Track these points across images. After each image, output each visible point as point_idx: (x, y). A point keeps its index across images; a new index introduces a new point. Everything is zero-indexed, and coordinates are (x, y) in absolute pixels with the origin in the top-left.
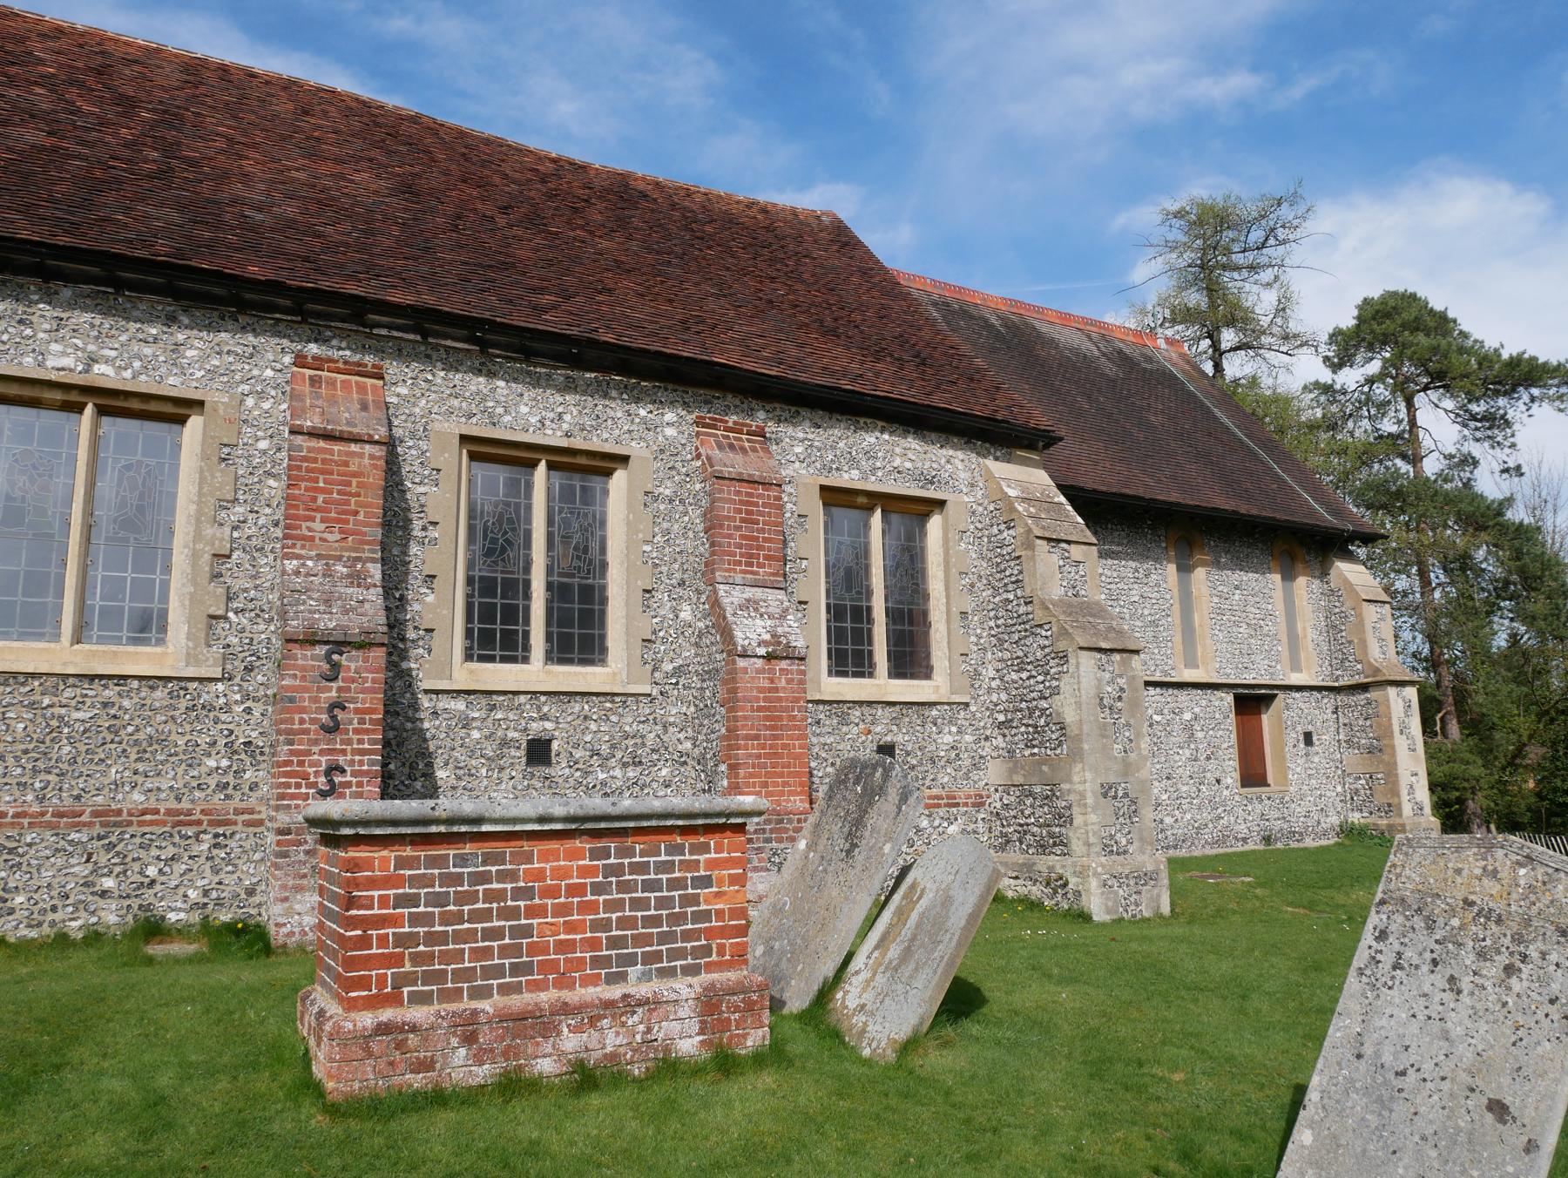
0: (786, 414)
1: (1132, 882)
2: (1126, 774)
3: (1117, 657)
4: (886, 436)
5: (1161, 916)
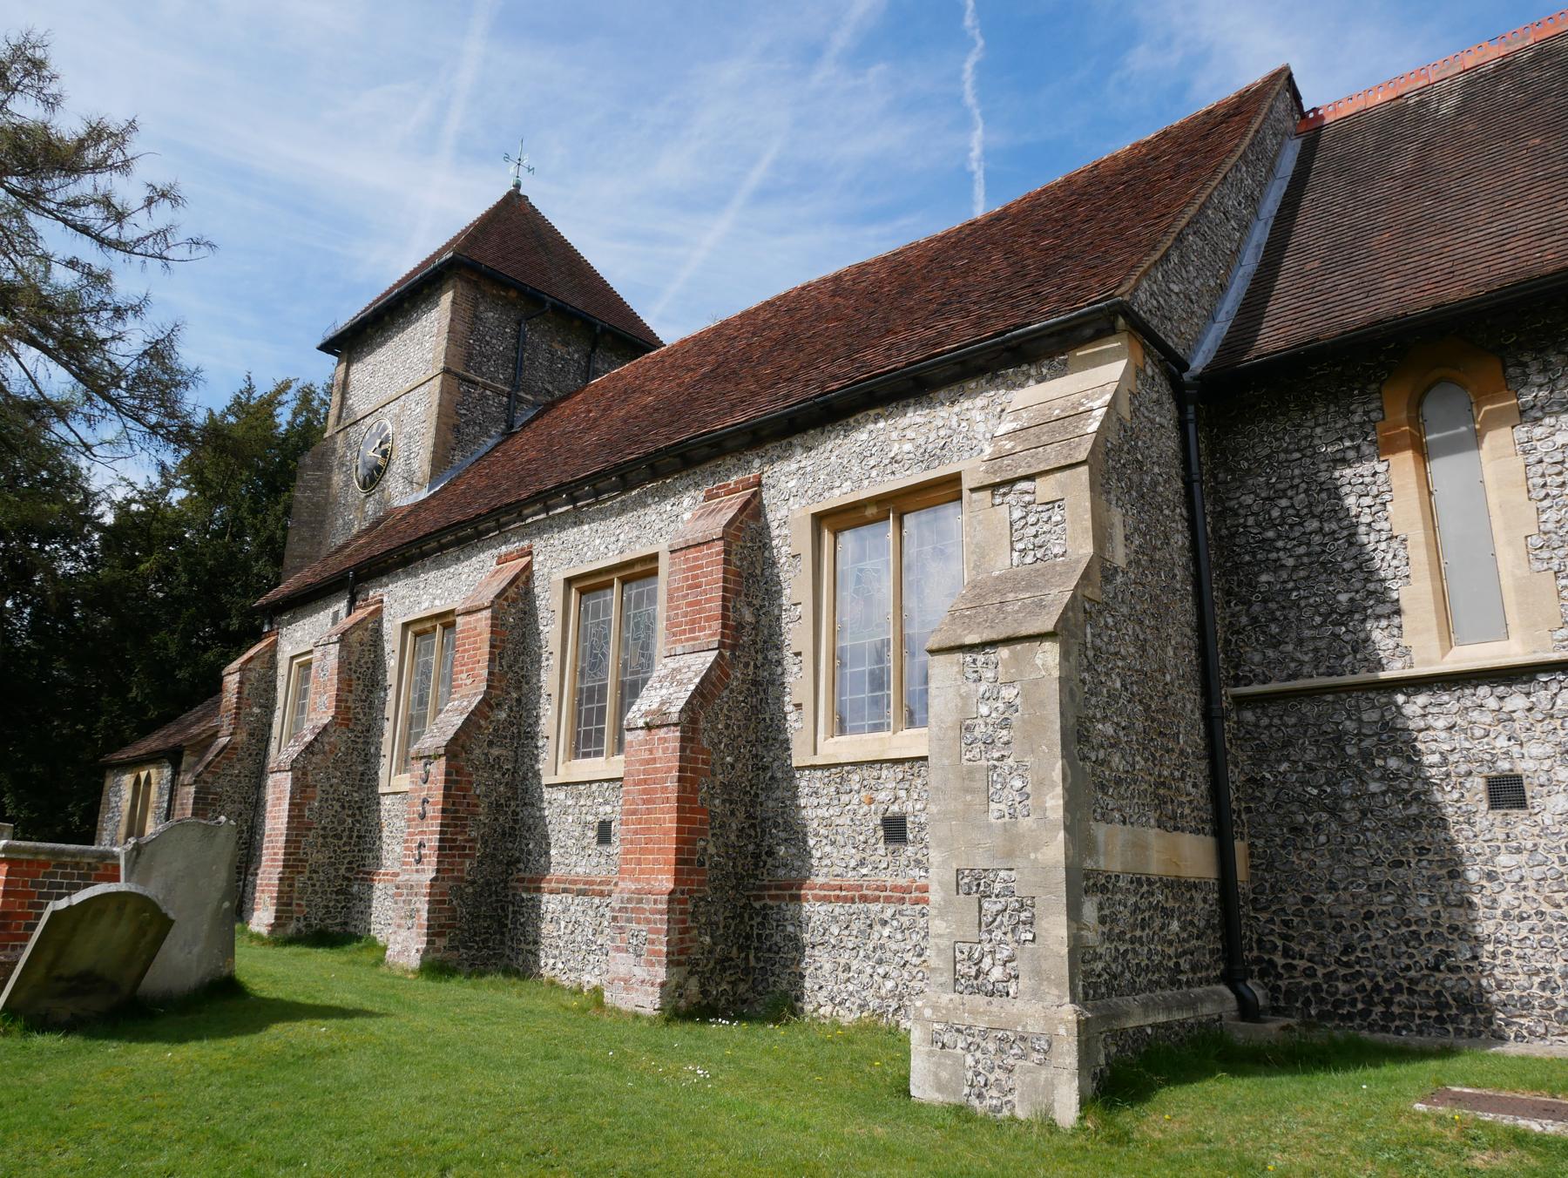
0: (778, 452)
1: (992, 1047)
2: (1010, 854)
3: (1004, 652)
4: (881, 424)
5: (1051, 1127)
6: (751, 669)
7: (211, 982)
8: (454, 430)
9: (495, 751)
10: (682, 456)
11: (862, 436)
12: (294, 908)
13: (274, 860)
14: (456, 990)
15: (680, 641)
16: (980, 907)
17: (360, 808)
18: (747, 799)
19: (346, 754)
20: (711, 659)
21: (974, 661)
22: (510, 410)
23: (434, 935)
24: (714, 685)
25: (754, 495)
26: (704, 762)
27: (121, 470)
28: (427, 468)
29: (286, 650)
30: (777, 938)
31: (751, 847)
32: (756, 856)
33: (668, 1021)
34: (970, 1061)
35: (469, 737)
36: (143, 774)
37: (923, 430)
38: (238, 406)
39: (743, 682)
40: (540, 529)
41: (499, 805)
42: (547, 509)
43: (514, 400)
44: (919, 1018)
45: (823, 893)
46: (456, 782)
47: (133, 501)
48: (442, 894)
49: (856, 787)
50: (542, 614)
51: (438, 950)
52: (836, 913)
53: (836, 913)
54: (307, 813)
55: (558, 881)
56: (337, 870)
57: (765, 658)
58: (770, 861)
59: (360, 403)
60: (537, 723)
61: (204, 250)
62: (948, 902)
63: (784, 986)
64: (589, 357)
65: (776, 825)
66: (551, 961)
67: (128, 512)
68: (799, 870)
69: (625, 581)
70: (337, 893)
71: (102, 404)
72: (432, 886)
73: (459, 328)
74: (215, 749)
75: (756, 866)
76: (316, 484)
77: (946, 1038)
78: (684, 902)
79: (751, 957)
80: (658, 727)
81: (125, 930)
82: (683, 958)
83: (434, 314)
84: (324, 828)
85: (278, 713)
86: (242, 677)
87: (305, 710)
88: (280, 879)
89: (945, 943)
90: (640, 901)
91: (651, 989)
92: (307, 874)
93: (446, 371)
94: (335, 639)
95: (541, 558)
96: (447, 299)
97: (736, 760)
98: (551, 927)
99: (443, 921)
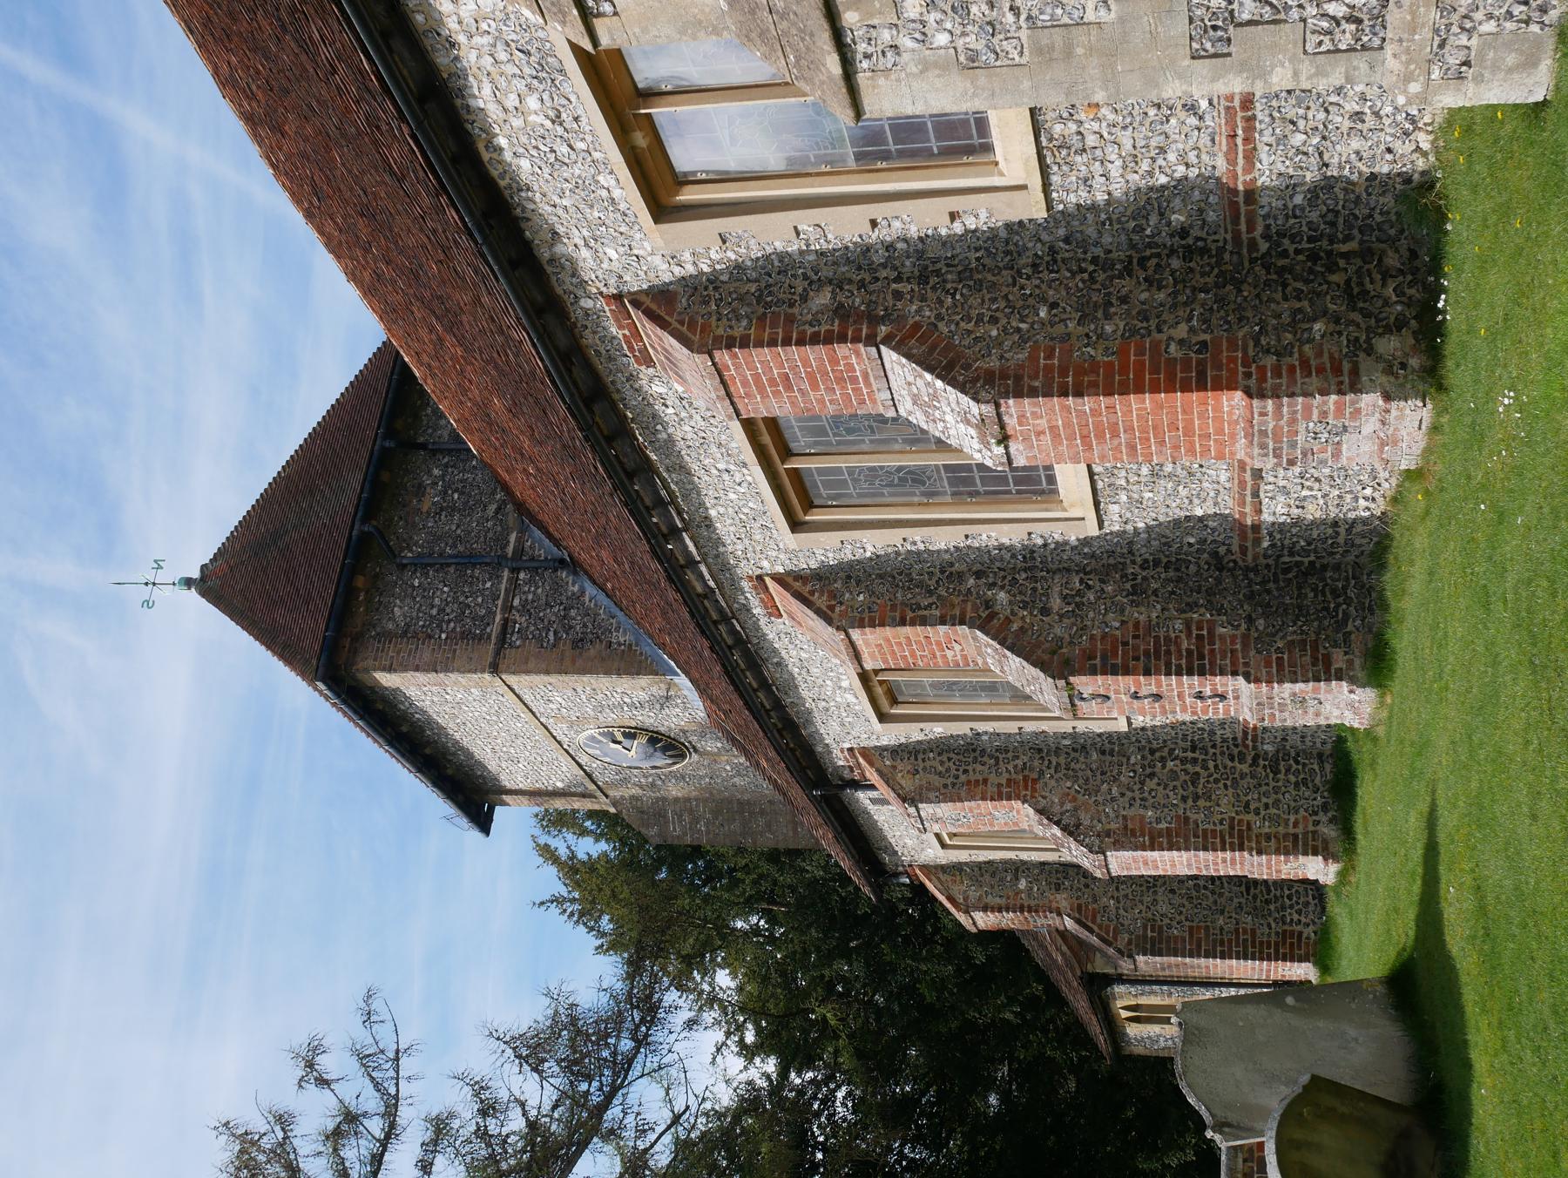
3: (850, 18)
4: (502, 141)
6: (904, 287)
7: (1396, 1008)
8: (582, 648)
9: (1056, 603)
10: (588, 402)
11: (525, 167)
12: (1300, 830)
13: (1233, 861)
14: (1405, 642)
15: (870, 394)
16: (1250, 23)
17: (1152, 752)
18: (1101, 277)
19: (1075, 779)
20: (895, 356)
21: (867, 56)
22: (537, 567)
23: (1327, 670)
24: (933, 348)
25: (636, 304)
26: (1050, 356)
27: (705, 1064)
28: (644, 681)
29: (933, 853)
30: (1314, 216)
31: (1175, 263)
32: (1189, 253)
33: (1441, 388)
34: (1490, 27)
35: (1038, 645)
36: (1124, 1014)
37: (502, 83)
38: (586, 915)
39: (923, 299)
40: (723, 568)
41: (1134, 591)
42: (692, 563)
43: (520, 560)
44: (1423, 98)
45: (1241, 161)
46: (1104, 658)
47: (741, 1042)
48: (1268, 664)
49: (1073, 127)
50: (847, 555)
51: (1350, 663)
52: (1271, 140)
53: (1271, 140)
54: (1163, 825)
55: (1243, 503)
56: (1243, 776)
57: (884, 265)
58: (1196, 232)
59: (560, 774)
60: (1009, 549)
61: (376, 1005)
62: (1243, 67)
63: (1388, 200)
64: (434, 452)
65: (1139, 229)
66: (1362, 503)
67: (755, 1045)
68: (1206, 193)
69: (787, 453)
70: (1276, 772)
71: (614, 1112)
72: (1257, 681)
73: (427, 656)
74: (1083, 934)
75: (1204, 251)
76: (686, 817)
77: (1453, 60)
78: (1262, 370)
79: (1344, 248)
80: (1002, 426)
81: (1328, 1137)
82: (1346, 366)
83: (412, 692)
84: (1184, 799)
85: (1024, 856)
86: (977, 909)
87: (1015, 829)
88: (1260, 853)
89: (1306, 68)
90: (1263, 433)
91: (1394, 413)
92: (1251, 817)
93: (495, 669)
94: (912, 810)
95: (765, 564)
96: (387, 679)
97: (1043, 300)
98: (1311, 508)
99: (1308, 659)
